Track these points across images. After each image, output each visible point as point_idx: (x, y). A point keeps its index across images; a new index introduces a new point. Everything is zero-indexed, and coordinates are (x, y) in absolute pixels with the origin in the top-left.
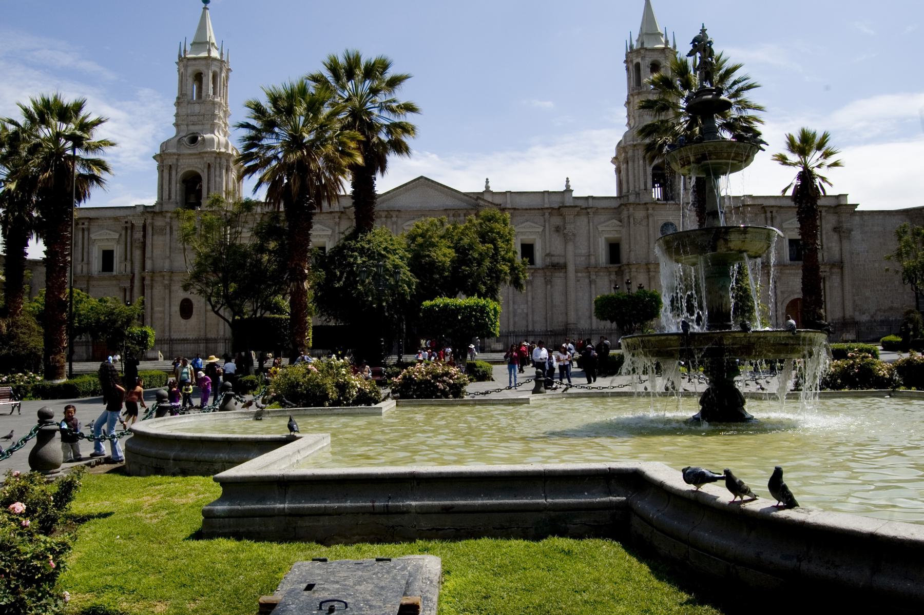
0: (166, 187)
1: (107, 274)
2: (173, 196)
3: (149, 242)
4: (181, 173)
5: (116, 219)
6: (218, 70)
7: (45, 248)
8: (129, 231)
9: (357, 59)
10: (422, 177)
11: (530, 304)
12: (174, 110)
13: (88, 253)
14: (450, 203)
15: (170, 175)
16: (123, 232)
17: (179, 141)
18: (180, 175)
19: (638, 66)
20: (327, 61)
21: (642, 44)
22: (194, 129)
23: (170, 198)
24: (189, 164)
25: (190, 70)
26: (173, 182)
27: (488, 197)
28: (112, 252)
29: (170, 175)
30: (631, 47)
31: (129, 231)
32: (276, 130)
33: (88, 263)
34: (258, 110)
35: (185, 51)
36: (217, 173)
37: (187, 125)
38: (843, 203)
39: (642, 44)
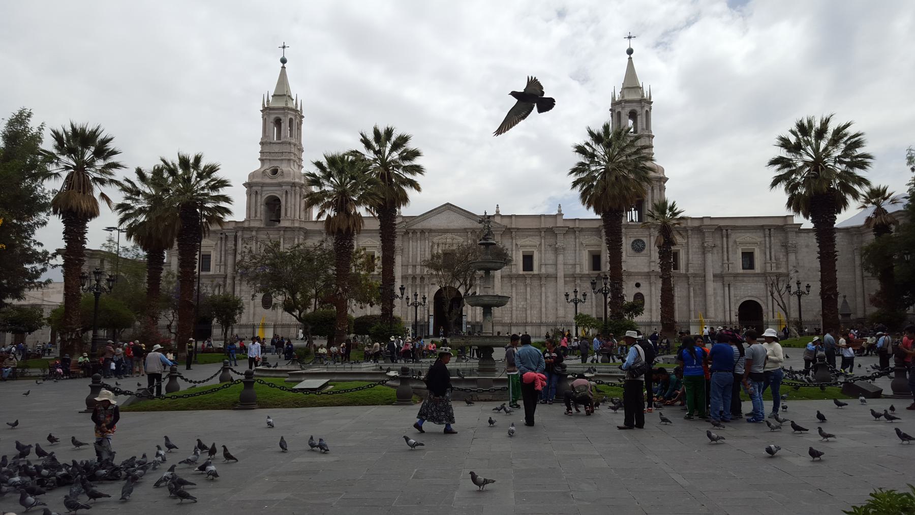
2: (258, 215)
7: (838, 216)
12: (259, 148)
14: (469, 224)
19: (619, 113)
21: (623, 97)
22: (275, 164)
23: (256, 216)
25: (273, 117)
26: (259, 204)
27: (498, 220)
32: (332, 179)
35: (268, 101)
38: (790, 222)
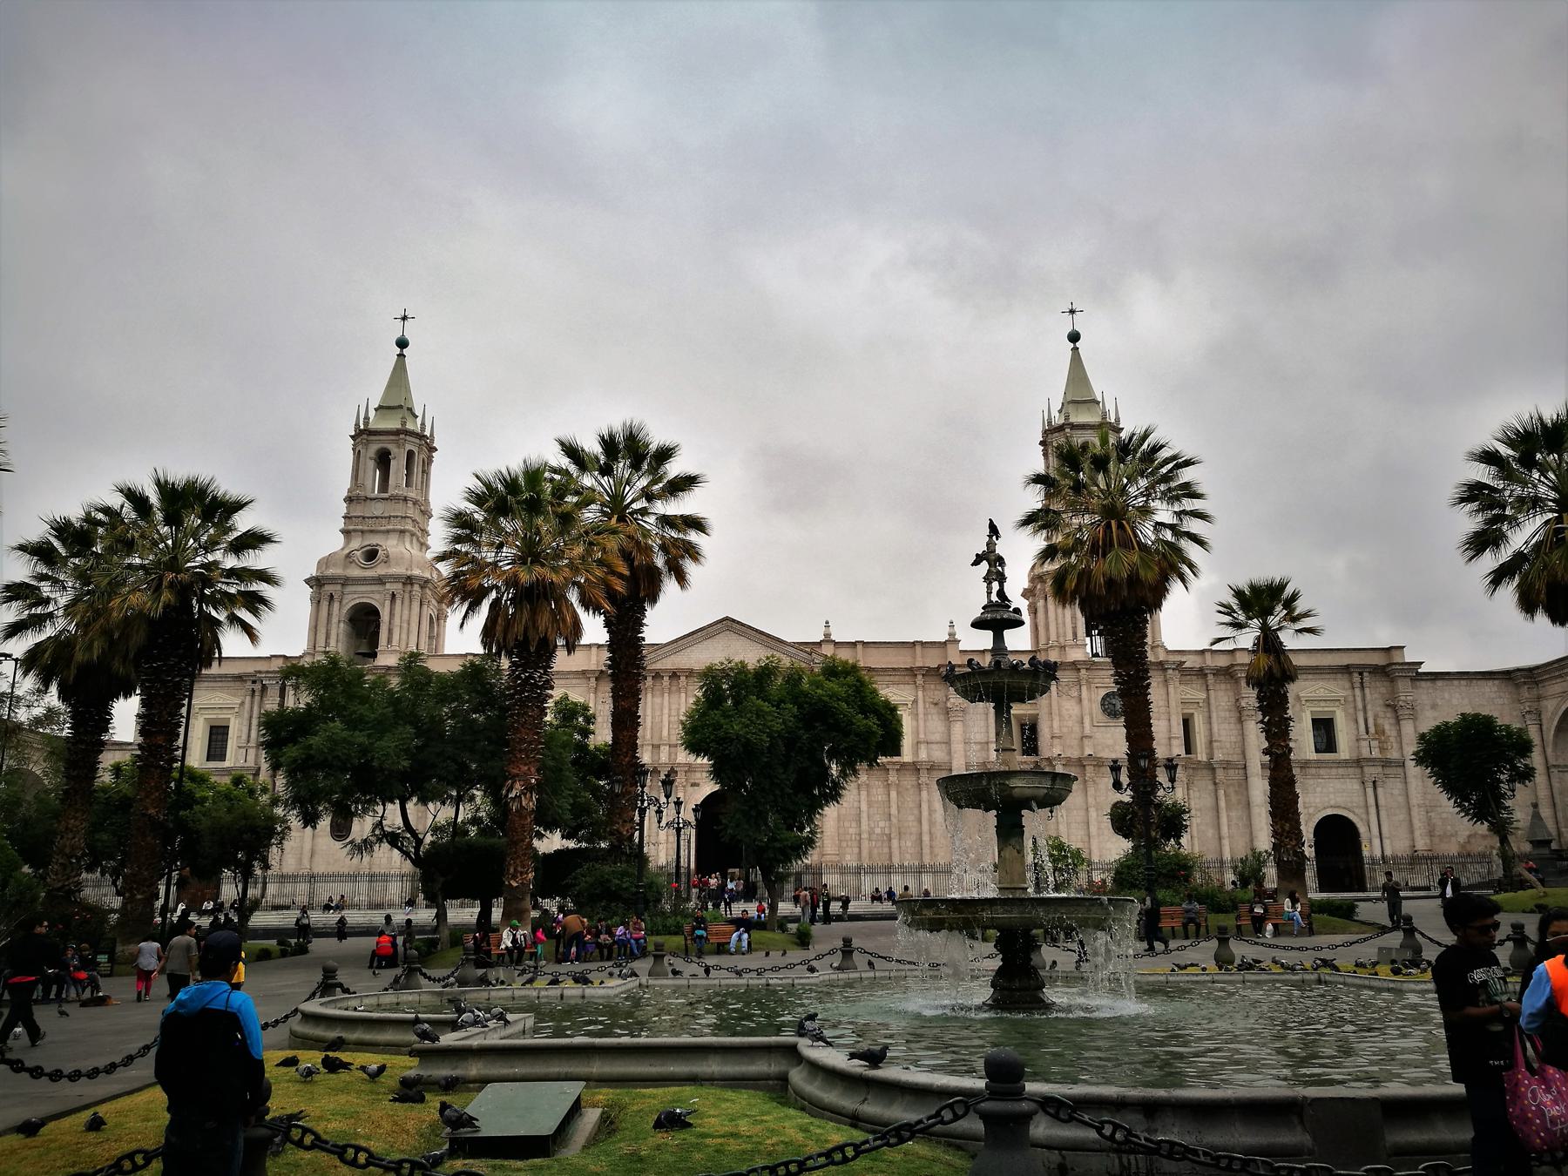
3: (1212, 701)
8: (257, 698)
9: (612, 436)
10: (727, 619)
11: (894, 820)
20: (605, 433)
21: (1067, 418)
26: (335, 620)
30: (1050, 423)
34: (1474, 493)
39: (1067, 418)
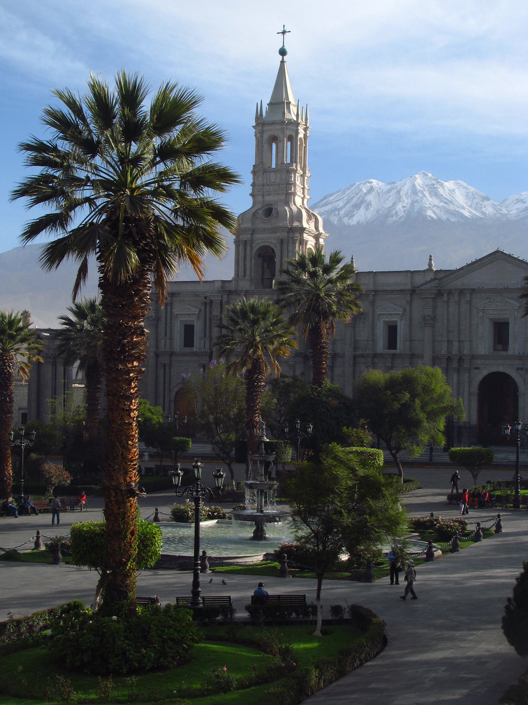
0: (241, 264)
1: (188, 350)
4: (256, 247)
5: (196, 295)
6: (293, 134)
13: (171, 327)
15: (245, 250)
16: (203, 308)
17: (254, 215)
18: (255, 250)
24: (263, 239)
26: (248, 259)
28: (192, 326)
29: (245, 250)
31: (208, 307)
33: (171, 339)
36: (290, 248)
37: (263, 196)
